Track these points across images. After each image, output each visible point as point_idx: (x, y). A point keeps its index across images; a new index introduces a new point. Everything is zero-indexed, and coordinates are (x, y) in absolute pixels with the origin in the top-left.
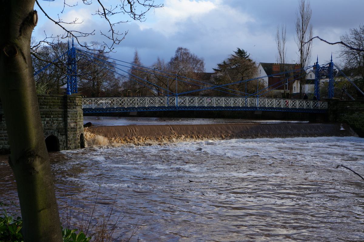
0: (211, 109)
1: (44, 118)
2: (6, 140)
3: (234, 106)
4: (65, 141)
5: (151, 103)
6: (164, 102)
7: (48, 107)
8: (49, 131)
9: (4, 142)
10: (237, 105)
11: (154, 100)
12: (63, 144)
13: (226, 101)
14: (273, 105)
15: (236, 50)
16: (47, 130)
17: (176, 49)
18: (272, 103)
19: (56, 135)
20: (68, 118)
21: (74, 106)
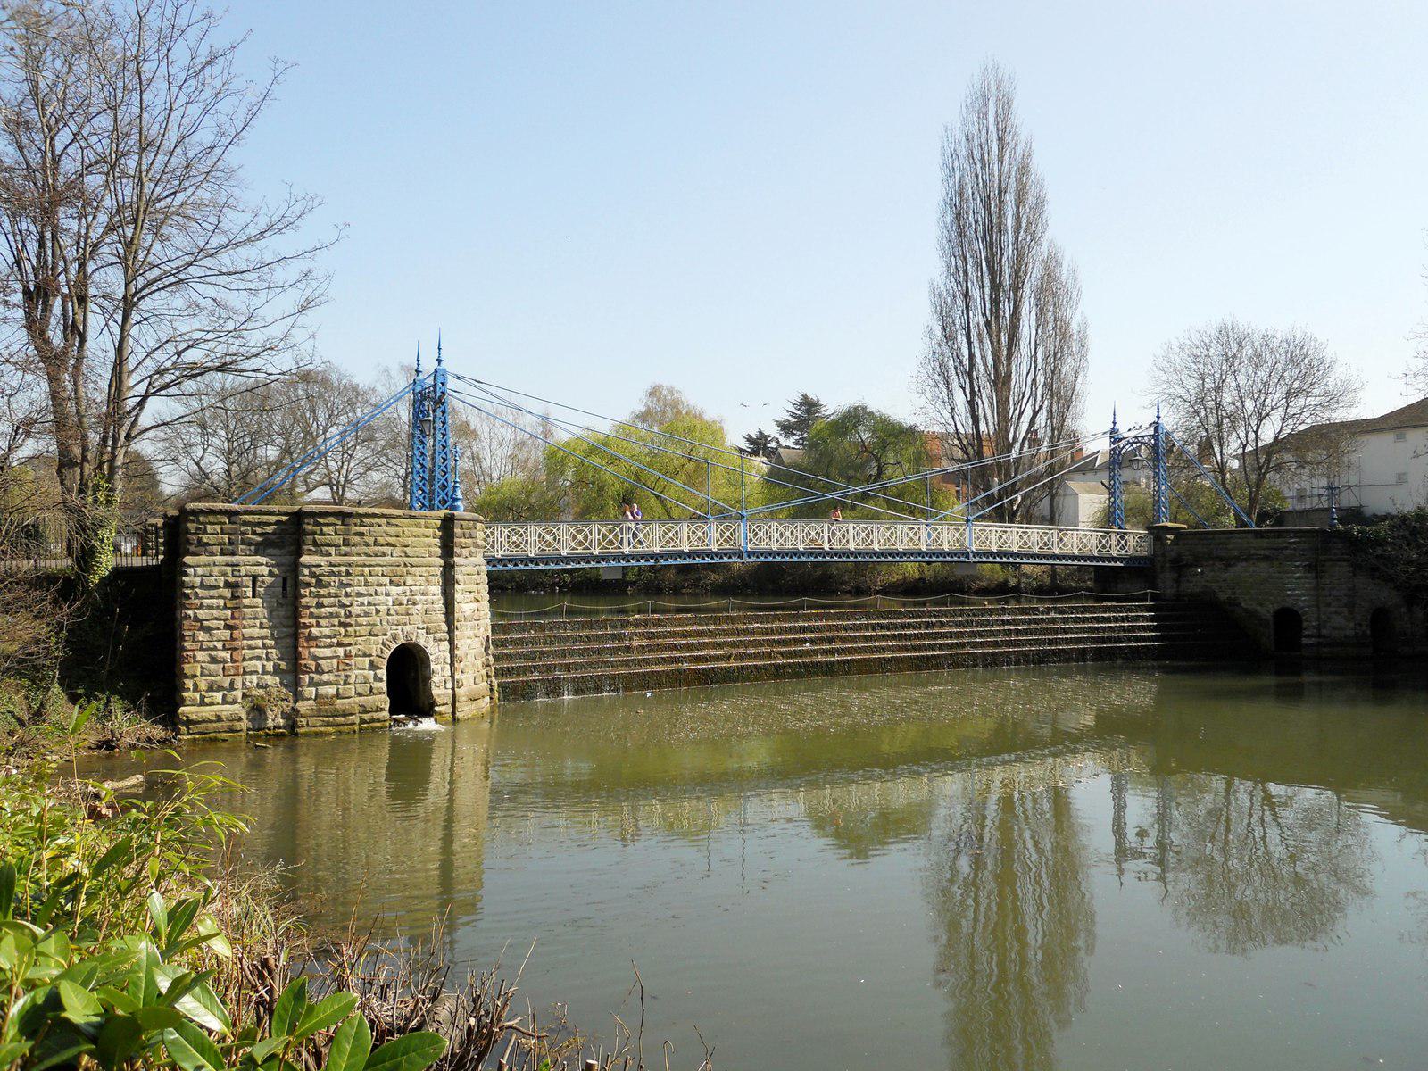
0: (694, 559)
1: (385, 585)
2: (268, 659)
3: (507, 553)
4: (448, 661)
5: (514, 543)
6: (555, 539)
7: (397, 551)
8: (399, 627)
9: (263, 666)
10: (788, 546)
11: (521, 535)
12: (443, 669)
13: (540, 534)
14: (872, 541)
15: (798, 399)
16: (393, 624)
17: (317, 366)
18: (844, 536)
19: (422, 642)
20: (457, 586)
21: (473, 549)
